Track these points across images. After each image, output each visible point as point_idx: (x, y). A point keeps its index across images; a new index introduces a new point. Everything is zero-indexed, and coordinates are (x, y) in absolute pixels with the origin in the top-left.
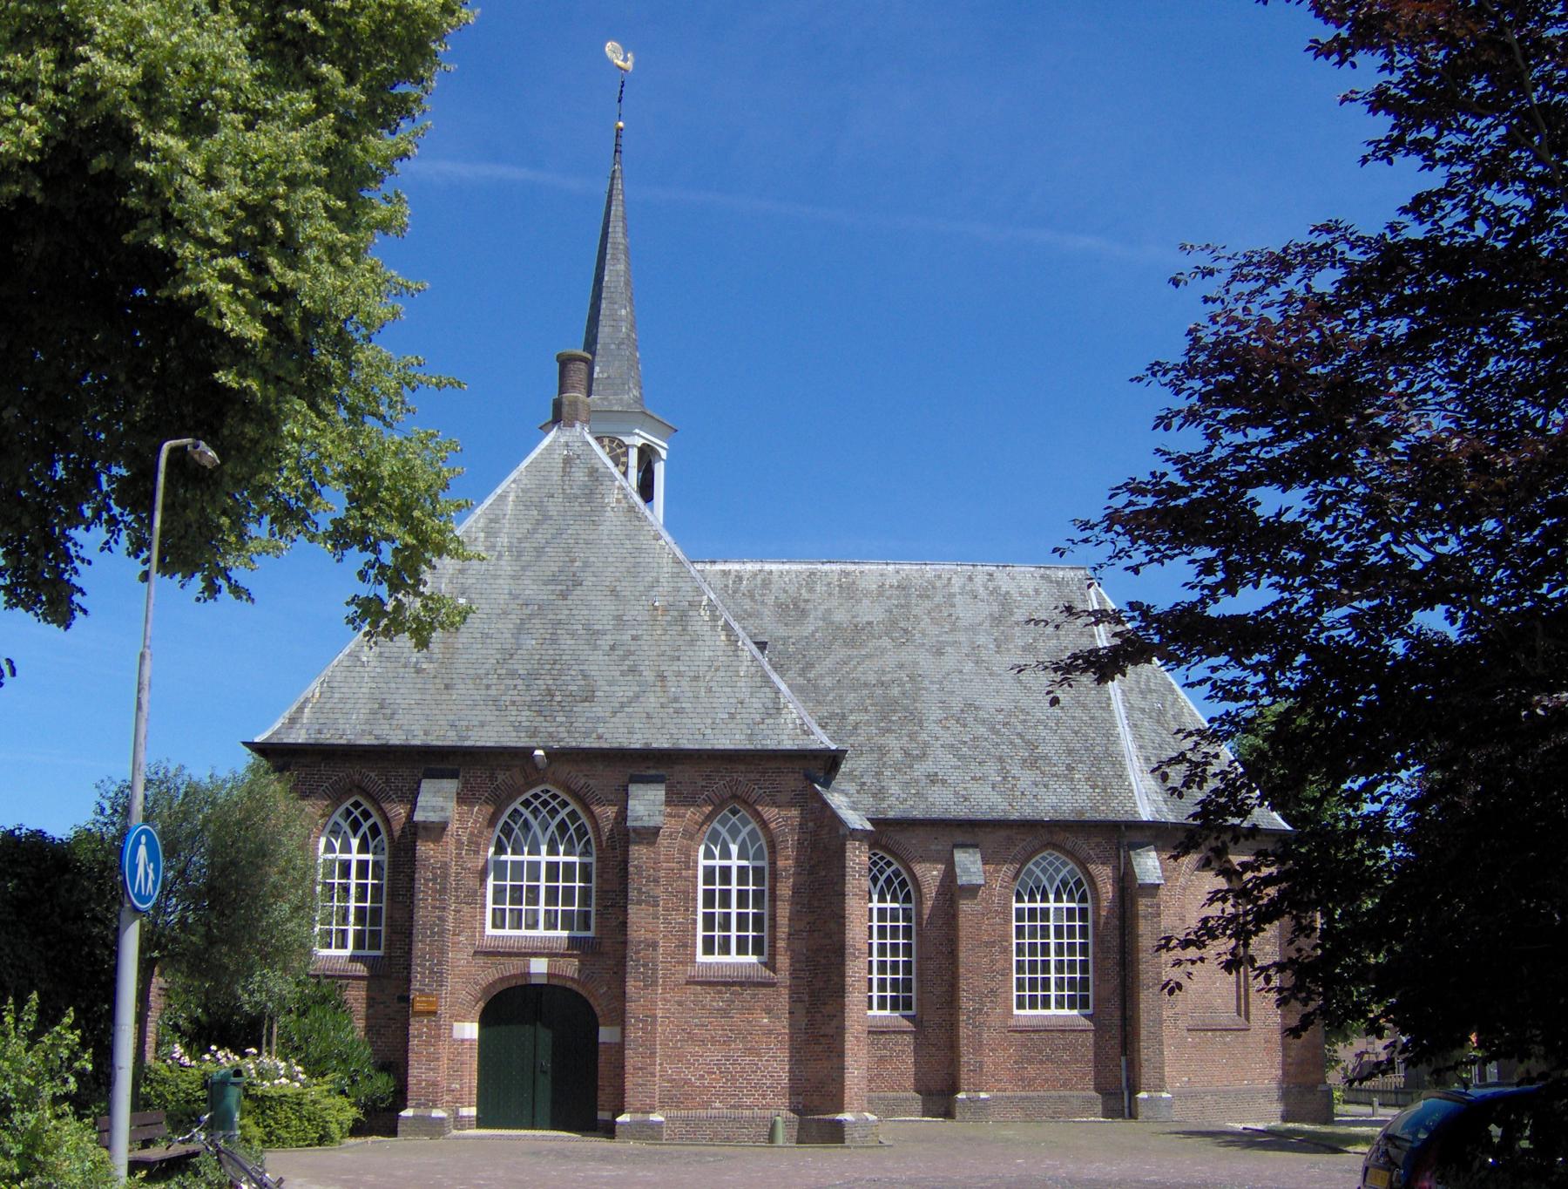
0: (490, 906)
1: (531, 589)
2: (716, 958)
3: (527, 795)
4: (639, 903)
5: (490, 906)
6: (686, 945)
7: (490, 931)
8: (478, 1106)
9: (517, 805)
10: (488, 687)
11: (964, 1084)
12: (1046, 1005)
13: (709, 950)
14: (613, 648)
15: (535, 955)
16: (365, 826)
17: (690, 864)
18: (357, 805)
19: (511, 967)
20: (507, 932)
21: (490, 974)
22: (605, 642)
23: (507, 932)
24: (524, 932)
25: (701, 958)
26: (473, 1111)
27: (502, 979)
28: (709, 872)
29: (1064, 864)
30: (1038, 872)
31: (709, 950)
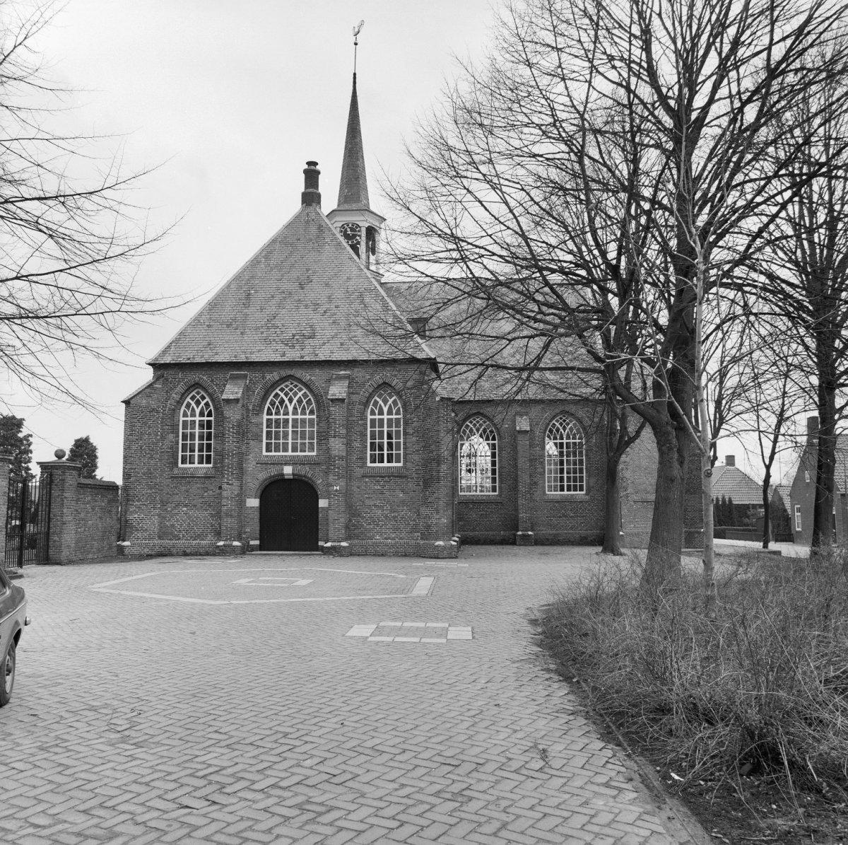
0: (265, 441)
1: (286, 286)
2: (394, 464)
3: (283, 386)
4: (335, 437)
5: (265, 441)
6: (363, 459)
7: (264, 453)
8: (260, 540)
9: (277, 391)
10: (262, 333)
11: (520, 528)
12: (562, 490)
13: (373, 461)
14: (325, 312)
15: (286, 464)
16: (203, 403)
17: (364, 418)
18: (198, 393)
19: (273, 471)
20: (273, 454)
21: (263, 476)
22: (321, 310)
23: (273, 454)
24: (281, 453)
25: (369, 464)
26: (257, 542)
27: (271, 477)
28: (373, 421)
29: (300, 390)
30: (282, 395)
31: (268, 450)
